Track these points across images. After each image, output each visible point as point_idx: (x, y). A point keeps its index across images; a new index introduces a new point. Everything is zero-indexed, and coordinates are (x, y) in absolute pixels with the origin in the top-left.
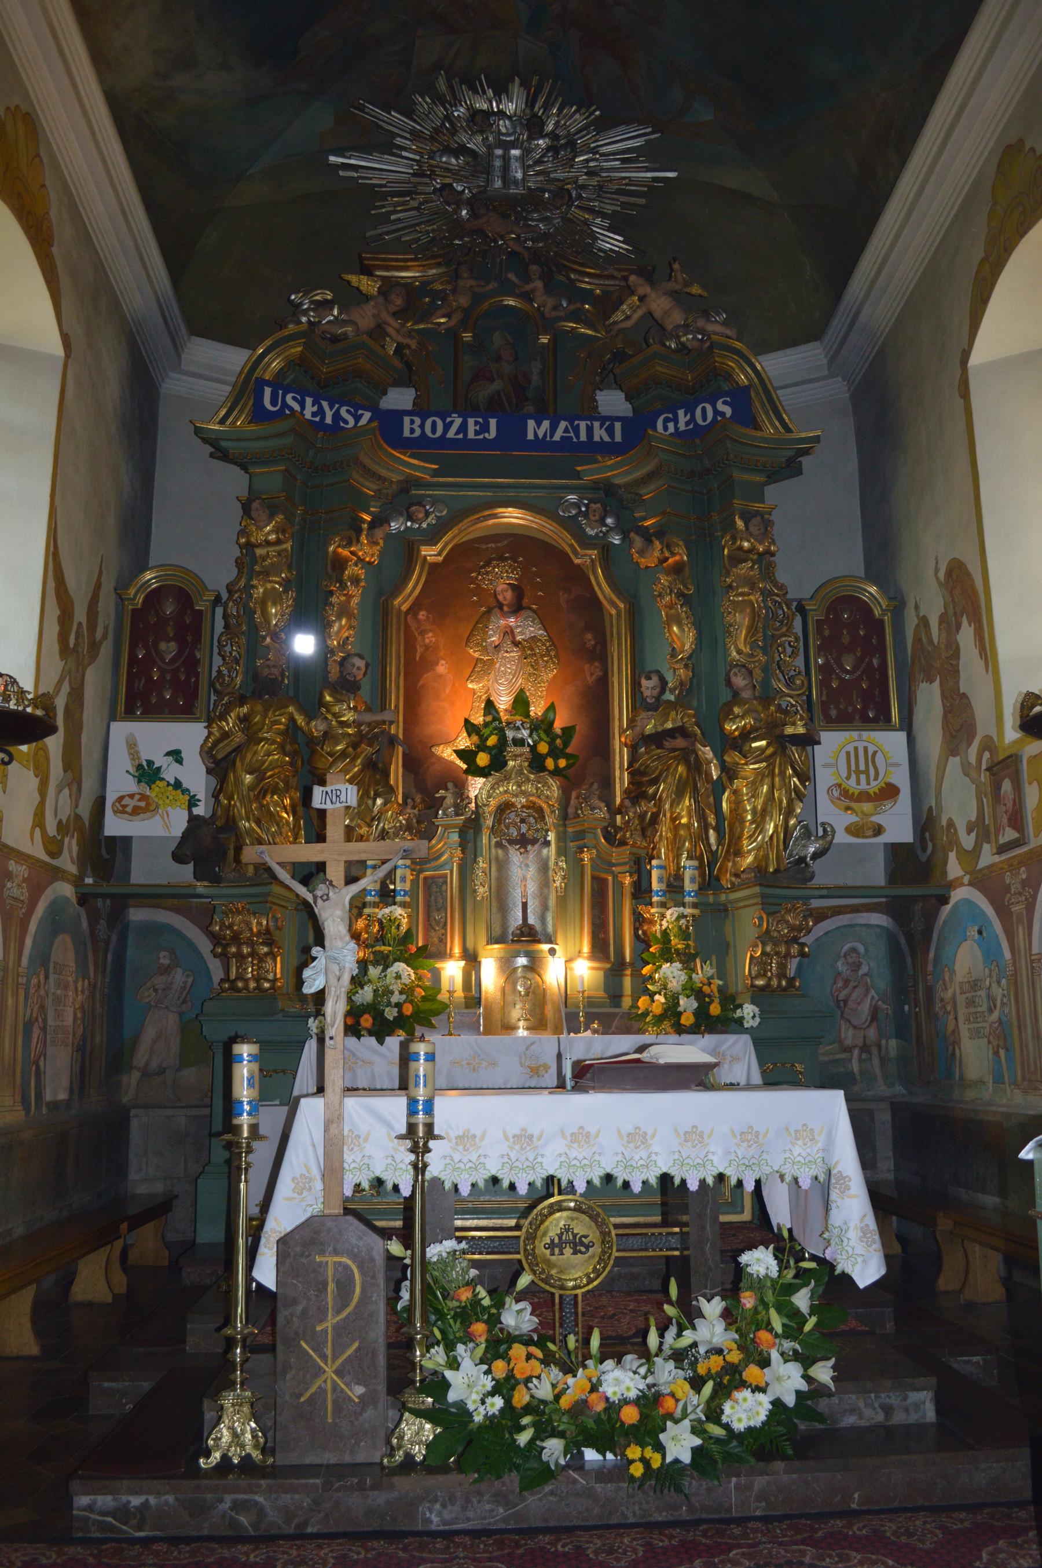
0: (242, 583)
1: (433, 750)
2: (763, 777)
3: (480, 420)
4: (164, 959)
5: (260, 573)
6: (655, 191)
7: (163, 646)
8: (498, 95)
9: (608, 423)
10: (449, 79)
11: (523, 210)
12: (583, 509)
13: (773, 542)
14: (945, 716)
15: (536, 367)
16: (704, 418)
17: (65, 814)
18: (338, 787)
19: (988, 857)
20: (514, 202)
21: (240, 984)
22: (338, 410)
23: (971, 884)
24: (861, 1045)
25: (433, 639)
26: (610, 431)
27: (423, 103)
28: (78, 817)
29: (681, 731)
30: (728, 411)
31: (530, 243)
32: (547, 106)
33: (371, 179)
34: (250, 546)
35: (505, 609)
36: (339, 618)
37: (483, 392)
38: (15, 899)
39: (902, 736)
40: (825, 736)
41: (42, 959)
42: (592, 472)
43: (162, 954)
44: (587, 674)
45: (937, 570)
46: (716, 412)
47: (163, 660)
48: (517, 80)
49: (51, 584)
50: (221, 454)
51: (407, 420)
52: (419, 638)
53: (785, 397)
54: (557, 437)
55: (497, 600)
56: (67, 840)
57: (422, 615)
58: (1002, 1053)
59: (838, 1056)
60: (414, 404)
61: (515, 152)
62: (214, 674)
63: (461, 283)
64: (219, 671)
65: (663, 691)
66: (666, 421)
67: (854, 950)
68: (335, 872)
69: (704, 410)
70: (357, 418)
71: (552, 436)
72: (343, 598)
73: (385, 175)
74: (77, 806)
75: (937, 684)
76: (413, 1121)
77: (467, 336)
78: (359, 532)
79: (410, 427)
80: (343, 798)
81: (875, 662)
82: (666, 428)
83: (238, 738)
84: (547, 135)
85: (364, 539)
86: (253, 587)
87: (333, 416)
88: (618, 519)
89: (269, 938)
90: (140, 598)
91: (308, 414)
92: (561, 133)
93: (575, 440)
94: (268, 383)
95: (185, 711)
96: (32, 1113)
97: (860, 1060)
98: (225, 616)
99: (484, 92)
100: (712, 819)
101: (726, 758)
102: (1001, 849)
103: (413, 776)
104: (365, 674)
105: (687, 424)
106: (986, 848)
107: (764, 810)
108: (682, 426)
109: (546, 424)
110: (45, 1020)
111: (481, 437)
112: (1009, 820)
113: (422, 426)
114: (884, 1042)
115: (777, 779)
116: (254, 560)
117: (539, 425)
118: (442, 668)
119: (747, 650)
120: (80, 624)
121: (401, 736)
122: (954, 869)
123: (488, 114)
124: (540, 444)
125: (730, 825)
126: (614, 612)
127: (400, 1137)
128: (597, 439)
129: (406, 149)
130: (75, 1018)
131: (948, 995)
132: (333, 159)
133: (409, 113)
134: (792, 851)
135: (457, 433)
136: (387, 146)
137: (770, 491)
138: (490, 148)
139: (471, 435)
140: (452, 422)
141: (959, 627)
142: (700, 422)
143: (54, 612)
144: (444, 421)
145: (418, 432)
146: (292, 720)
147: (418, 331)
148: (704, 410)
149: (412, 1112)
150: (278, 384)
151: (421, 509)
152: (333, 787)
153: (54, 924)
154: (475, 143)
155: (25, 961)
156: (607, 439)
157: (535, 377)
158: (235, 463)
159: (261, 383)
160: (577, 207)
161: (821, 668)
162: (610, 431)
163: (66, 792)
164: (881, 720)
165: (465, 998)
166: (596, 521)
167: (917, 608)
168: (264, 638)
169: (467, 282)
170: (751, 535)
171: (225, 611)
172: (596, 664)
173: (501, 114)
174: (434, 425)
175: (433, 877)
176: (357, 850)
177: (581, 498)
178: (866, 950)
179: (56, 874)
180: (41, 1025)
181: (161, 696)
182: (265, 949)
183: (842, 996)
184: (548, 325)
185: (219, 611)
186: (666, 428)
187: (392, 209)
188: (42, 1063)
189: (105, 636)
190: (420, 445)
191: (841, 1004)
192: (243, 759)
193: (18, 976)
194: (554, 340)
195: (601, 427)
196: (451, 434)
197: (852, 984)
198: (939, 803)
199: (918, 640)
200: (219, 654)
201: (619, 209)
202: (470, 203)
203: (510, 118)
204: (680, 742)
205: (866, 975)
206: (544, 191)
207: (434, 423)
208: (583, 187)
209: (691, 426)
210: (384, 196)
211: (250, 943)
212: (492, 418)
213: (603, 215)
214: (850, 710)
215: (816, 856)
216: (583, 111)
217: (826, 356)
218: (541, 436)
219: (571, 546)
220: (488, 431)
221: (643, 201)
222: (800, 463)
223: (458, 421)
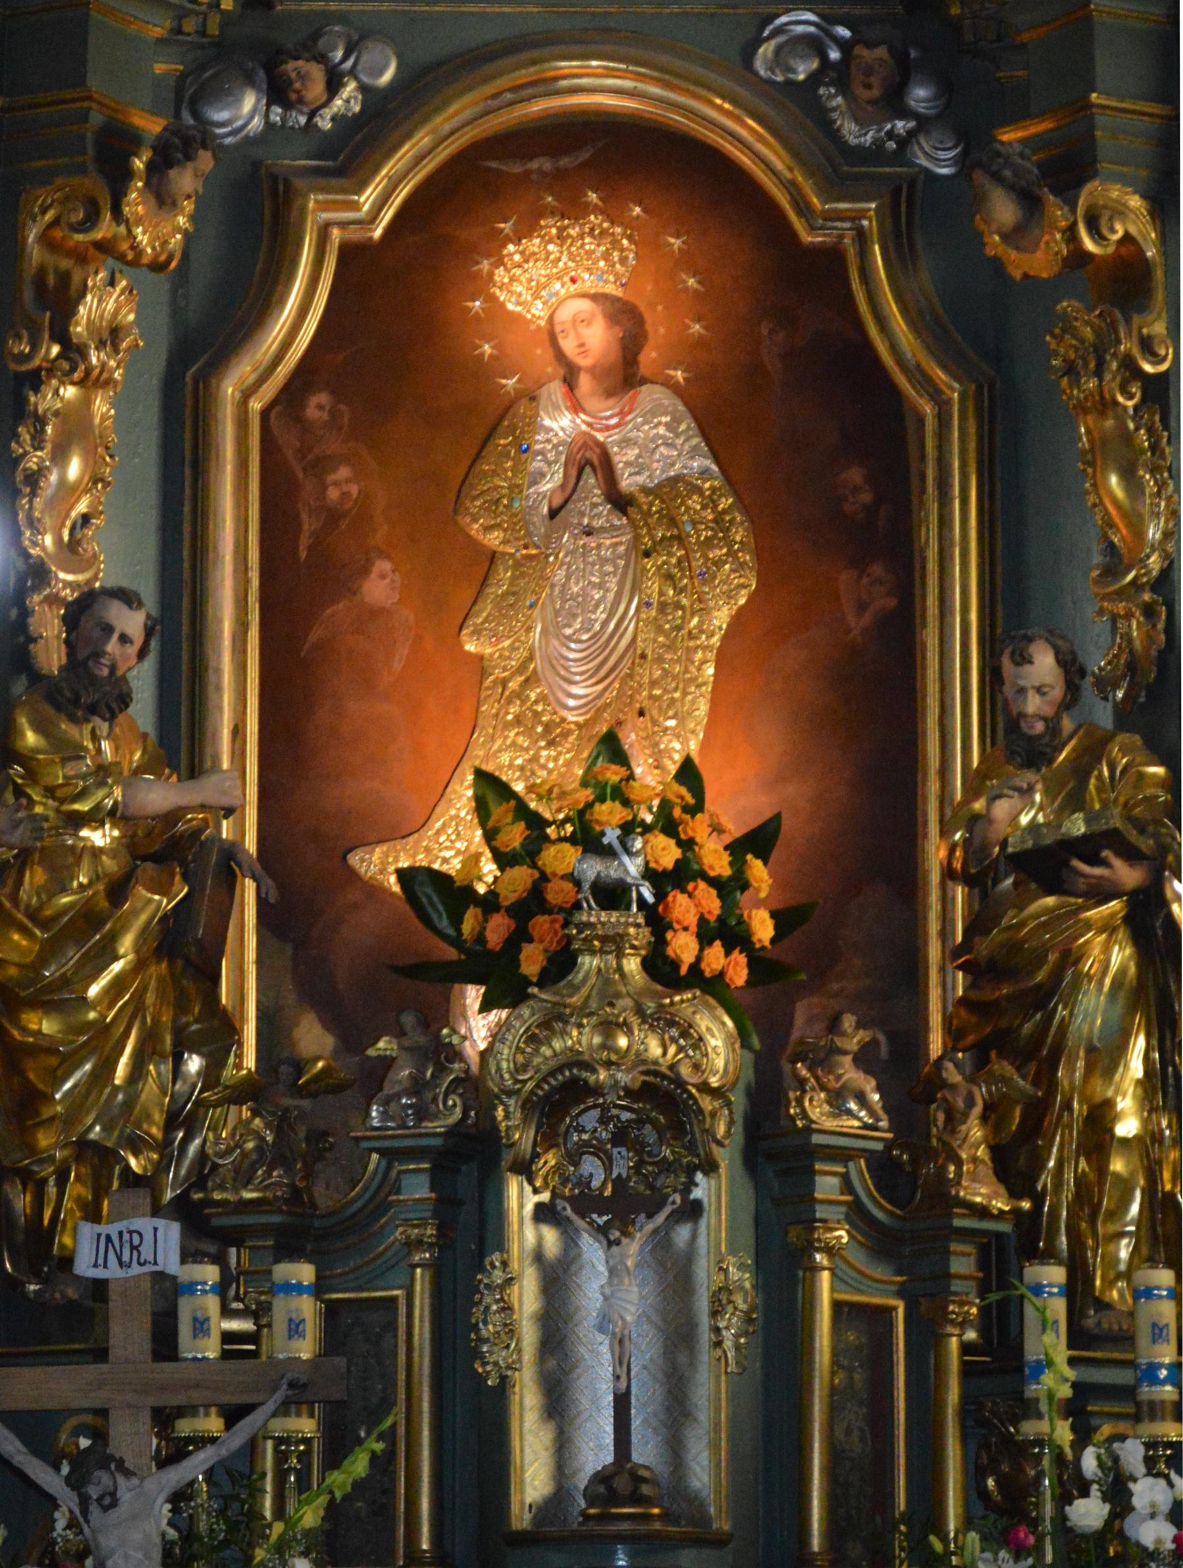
1: (354, 859)
12: (834, 55)
25: (354, 490)
35: (585, 383)
52: (309, 485)
55: (560, 356)
78: (119, 180)
80: (146, 1252)
88: (947, 89)
104: (142, 654)
121: (251, 844)
166: (871, 102)
172: (877, 570)
177: (830, 19)
219: (791, 187)
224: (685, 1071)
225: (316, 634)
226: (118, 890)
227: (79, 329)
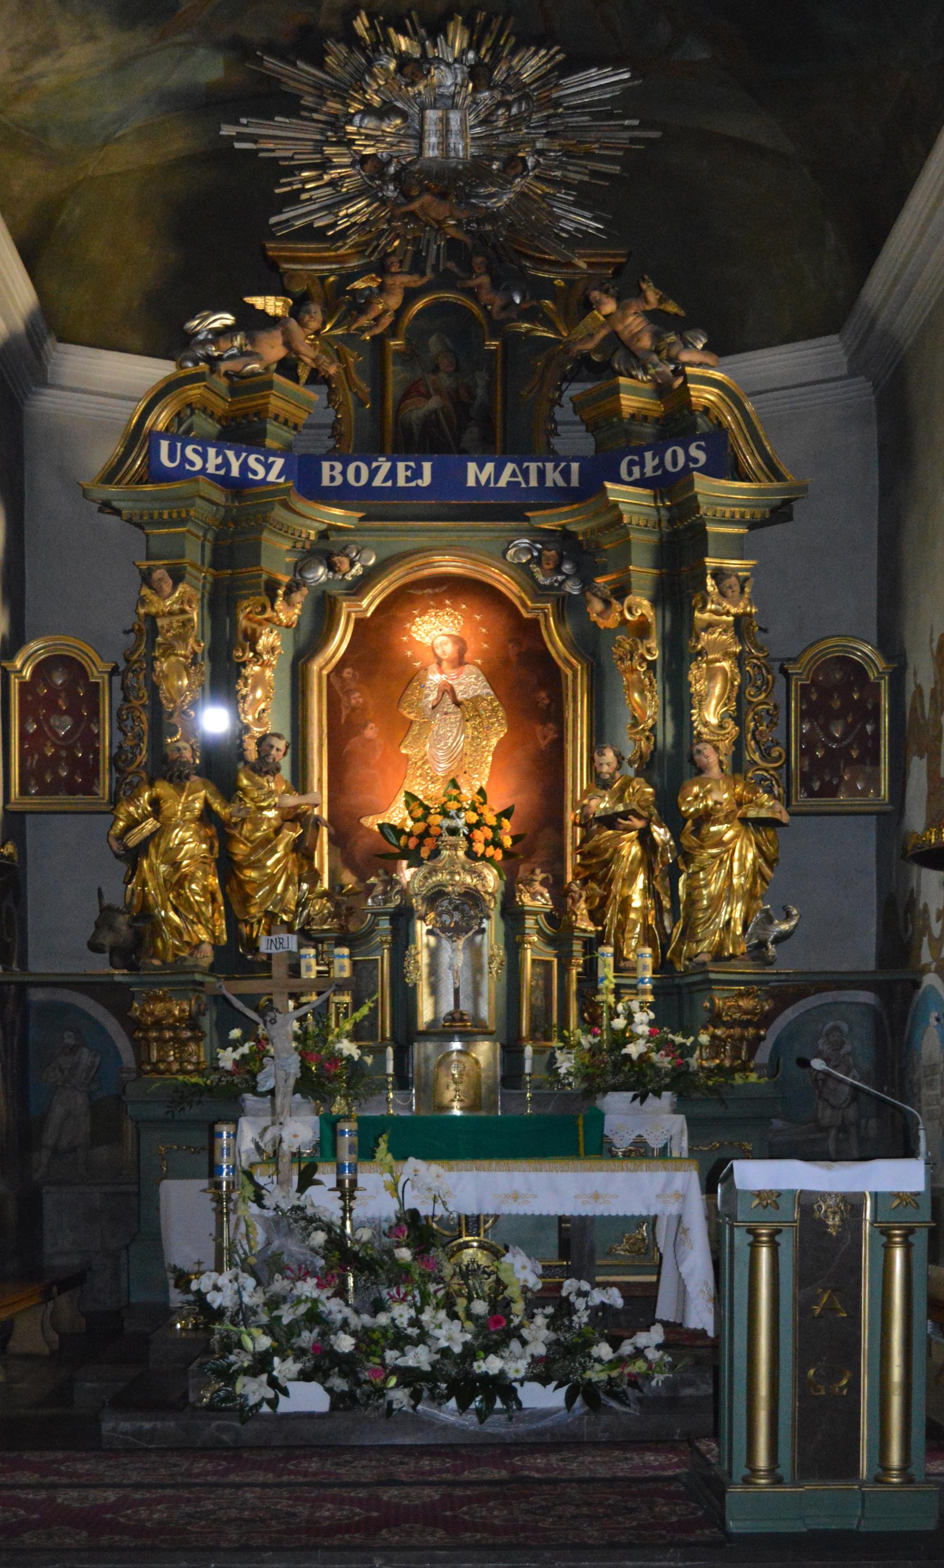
1: (362, 821)
3: (412, 464)
4: (69, 1038)
7: (54, 721)
9: (563, 464)
11: (466, 184)
15: (481, 379)
16: (675, 464)
18: (282, 935)
21: (162, 1067)
22: (246, 459)
25: (361, 700)
26: (566, 474)
30: (702, 457)
33: (273, 150)
43: (67, 1034)
44: (539, 737)
45: (931, 641)
46: (689, 458)
47: (56, 735)
51: (326, 465)
52: (344, 699)
54: (502, 483)
55: (436, 655)
59: (812, 1136)
66: (631, 464)
67: (836, 1028)
69: (674, 454)
71: (496, 481)
75: (925, 760)
78: (273, 598)
80: (285, 944)
81: (869, 728)
87: (241, 466)
89: (192, 1022)
91: (211, 469)
93: (523, 485)
100: (666, 903)
103: (339, 850)
104: (285, 754)
105: (655, 469)
108: (649, 472)
109: (490, 467)
111: (413, 484)
113: (344, 473)
117: (481, 468)
118: (371, 732)
122: (926, 956)
135: (385, 480)
139: (401, 482)
140: (378, 468)
142: (670, 468)
144: (369, 465)
145: (339, 481)
148: (674, 454)
156: (561, 483)
159: (155, 437)
161: (802, 738)
162: (566, 474)
167: (915, 674)
169: (402, 281)
174: (358, 470)
178: (851, 1029)
182: (189, 1034)
185: (117, 680)
187: (300, 186)
192: (157, 847)
194: (505, 345)
195: (555, 468)
196: (378, 482)
198: (919, 884)
201: (586, 178)
205: (849, 1054)
207: (358, 470)
209: (659, 472)
211: (172, 1028)
212: (428, 461)
216: (543, 52)
217: (845, 353)
218: (483, 481)
219: (520, 598)
220: (421, 477)
221: (616, 169)
223: (386, 466)
224: (479, 887)
225: (348, 748)
226: (278, 831)
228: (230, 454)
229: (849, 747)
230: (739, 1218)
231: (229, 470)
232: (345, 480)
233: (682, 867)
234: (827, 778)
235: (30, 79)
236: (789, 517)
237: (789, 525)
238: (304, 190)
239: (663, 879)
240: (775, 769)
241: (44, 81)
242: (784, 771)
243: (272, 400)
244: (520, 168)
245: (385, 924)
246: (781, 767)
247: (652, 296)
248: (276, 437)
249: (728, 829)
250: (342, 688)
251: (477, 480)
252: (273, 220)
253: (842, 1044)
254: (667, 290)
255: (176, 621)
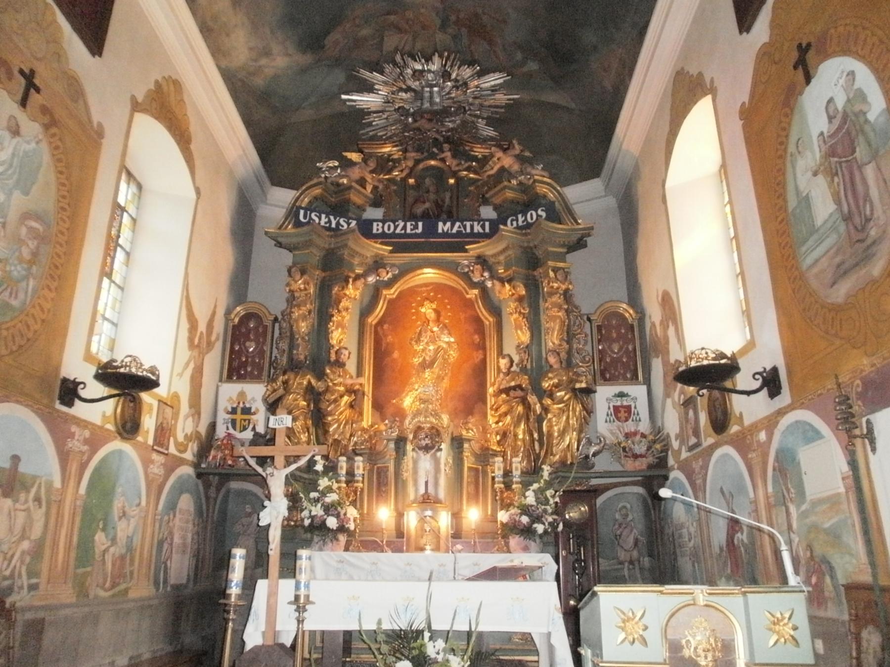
0: (288, 310)
2: (564, 412)
3: (414, 223)
5: (296, 306)
6: (511, 107)
8: (427, 61)
9: (481, 223)
10: (402, 56)
13: (571, 283)
14: (664, 377)
15: (448, 195)
16: (532, 219)
17: (189, 430)
19: (684, 455)
20: (435, 113)
23: (678, 469)
24: (628, 560)
26: (483, 227)
27: (388, 68)
28: (198, 432)
29: (519, 387)
30: (544, 214)
31: (444, 133)
32: (452, 66)
34: (292, 292)
36: (337, 328)
37: (419, 209)
38: (154, 474)
39: (644, 388)
40: (599, 389)
41: (172, 506)
42: (474, 249)
43: (247, 506)
45: (657, 296)
47: (248, 351)
48: (437, 54)
49: (184, 312)
50: (279, 245)
51: (375, 224)
52: (384, 338)
53: (577, 209)
56: (190, 444)
57: (386, 326)
58: (696, 565)
59: (616, 567)
60: (384, 216)
61: (436, 89)
62: (273, 358)
63: (408, 154)
64: (276, 357)
65: (511, 365)
66: (512, 221)
67: (625, 507)
68: (279, 460)
69: (531, 215)
70: (349, 224)
72: (340, 318)
73: (369, 103)
74: (197, 427)
75: (660, 358)
76: (298, 593)
77: (411, 181)
78: (347, 282)
79: (377, 228)
80: (284, 422)
82: (512, 224)
83: (281, 391)
84: (453, 80)
85: (350, 286)
86: (292, 312)
90: (237, 320)
91: (322, 223)
92: (459, 78)
94: (302, 208)
95: (255, 378)
96: (160, 590)
97: (629, 569)
98: (280, 328)
99: (420, 61)
100: (536, 436)
101: (544, 402)
102: (691, 449)
105: (523, 222)
106: (683, 448)
107: (564, 429)
108: (520, 223)
110: (172, 539)
111: (414, 232)
112: (693, 432)
113: (383, 227)
114: (641, 559)
115: (571, 413)
116: (294, 298)
119: (557, 342)
120: (202, 333)
123: (422, 72)
124: (445, 235)
125: (547, 438)
126: (487, 323)
127: (290, 603)
128: (476, 231)
129: (380, 90)
130: (193, 539)
131: (670, 532)
132: (344, 97)
133: (382, 73)
134: (581, 452)
135: (402, 230)
136: (369, 88)
137: (569, 257)
138: (423, 87)
139: (408, 231)
140: (398, 225)
141: (668, 327)
143: (185, 325)
145: (380, 231)
146: (309, 383)
147: (386, 179)
148: (531, 215)
149: (297, 587)
150: (308, 209)
151: (384, 270)
152: (279, 417)
153: (180, 488)
154: (415, 85)
155: (160, 507)
157: (447, 200)
158: (285, 248)
160: (470, 115)
162: (483, 227)
163: (190, 419)
164: (634, 379)
165: (508, 539)
167: (650, 317)
168: (298, 339)
169: (412, 155)
170: (558, 280)
171: (280, 325)
173: (429, 71)
175: (381, 467)
176: (293, 450)
179: (182, 462)
180: (170, 542)
181: (246, 370)
183: (618, 532)
184: (454, 174)
186: (512, 224)
188: (169, 563)
189: (217, 339)
190: (383, 237)
191: (618, 537)
193: (155, 515)
196: (398, 231)
197: (624, 526)
198: (663, 424)
199: (651, 335)
200: (276, 348)
202: (413, 115)
203: (433, 72)
204: (519, 393)
206: (451, 107)
208: (471, 104)
210: (369, 113)
213: (483, 118)
214: (617, 373)
215: (594, 455)
220: (417, 228)
222: (586, 241)
224: (439, 424)
225: (385, 362)
226: (342, 396)
227: (340, 307)
228: (332, 218)
229: (622, 357)
230: (605, 659)
231: (331, 224)
232: (383, 231)
233: (545, 416)
234: (613, 372)
235: (260, 67)
236: (585, 246)
237: (586, 249)
238: (374, 121)
239: (534, 423)
240: (587, 367)
241: (266, 70)
242: (592, 367)
243: (351, 195)
244: (463, 110)
245: (392, 445)
246: (590, 366)
247: (517, 148)
248: (354, 213)
249: (566, 394)
250: (383, 334)
251: (443, 230)
252: (362, 132)
253: (627, 515)
254: (525, 147)
255: (303, 294)
